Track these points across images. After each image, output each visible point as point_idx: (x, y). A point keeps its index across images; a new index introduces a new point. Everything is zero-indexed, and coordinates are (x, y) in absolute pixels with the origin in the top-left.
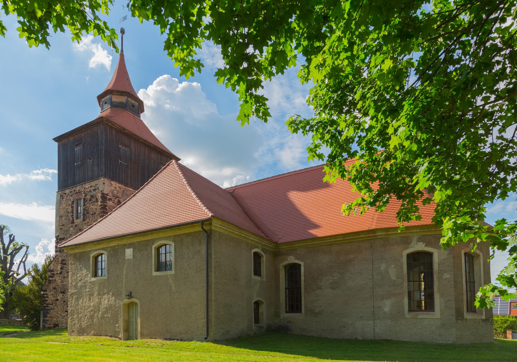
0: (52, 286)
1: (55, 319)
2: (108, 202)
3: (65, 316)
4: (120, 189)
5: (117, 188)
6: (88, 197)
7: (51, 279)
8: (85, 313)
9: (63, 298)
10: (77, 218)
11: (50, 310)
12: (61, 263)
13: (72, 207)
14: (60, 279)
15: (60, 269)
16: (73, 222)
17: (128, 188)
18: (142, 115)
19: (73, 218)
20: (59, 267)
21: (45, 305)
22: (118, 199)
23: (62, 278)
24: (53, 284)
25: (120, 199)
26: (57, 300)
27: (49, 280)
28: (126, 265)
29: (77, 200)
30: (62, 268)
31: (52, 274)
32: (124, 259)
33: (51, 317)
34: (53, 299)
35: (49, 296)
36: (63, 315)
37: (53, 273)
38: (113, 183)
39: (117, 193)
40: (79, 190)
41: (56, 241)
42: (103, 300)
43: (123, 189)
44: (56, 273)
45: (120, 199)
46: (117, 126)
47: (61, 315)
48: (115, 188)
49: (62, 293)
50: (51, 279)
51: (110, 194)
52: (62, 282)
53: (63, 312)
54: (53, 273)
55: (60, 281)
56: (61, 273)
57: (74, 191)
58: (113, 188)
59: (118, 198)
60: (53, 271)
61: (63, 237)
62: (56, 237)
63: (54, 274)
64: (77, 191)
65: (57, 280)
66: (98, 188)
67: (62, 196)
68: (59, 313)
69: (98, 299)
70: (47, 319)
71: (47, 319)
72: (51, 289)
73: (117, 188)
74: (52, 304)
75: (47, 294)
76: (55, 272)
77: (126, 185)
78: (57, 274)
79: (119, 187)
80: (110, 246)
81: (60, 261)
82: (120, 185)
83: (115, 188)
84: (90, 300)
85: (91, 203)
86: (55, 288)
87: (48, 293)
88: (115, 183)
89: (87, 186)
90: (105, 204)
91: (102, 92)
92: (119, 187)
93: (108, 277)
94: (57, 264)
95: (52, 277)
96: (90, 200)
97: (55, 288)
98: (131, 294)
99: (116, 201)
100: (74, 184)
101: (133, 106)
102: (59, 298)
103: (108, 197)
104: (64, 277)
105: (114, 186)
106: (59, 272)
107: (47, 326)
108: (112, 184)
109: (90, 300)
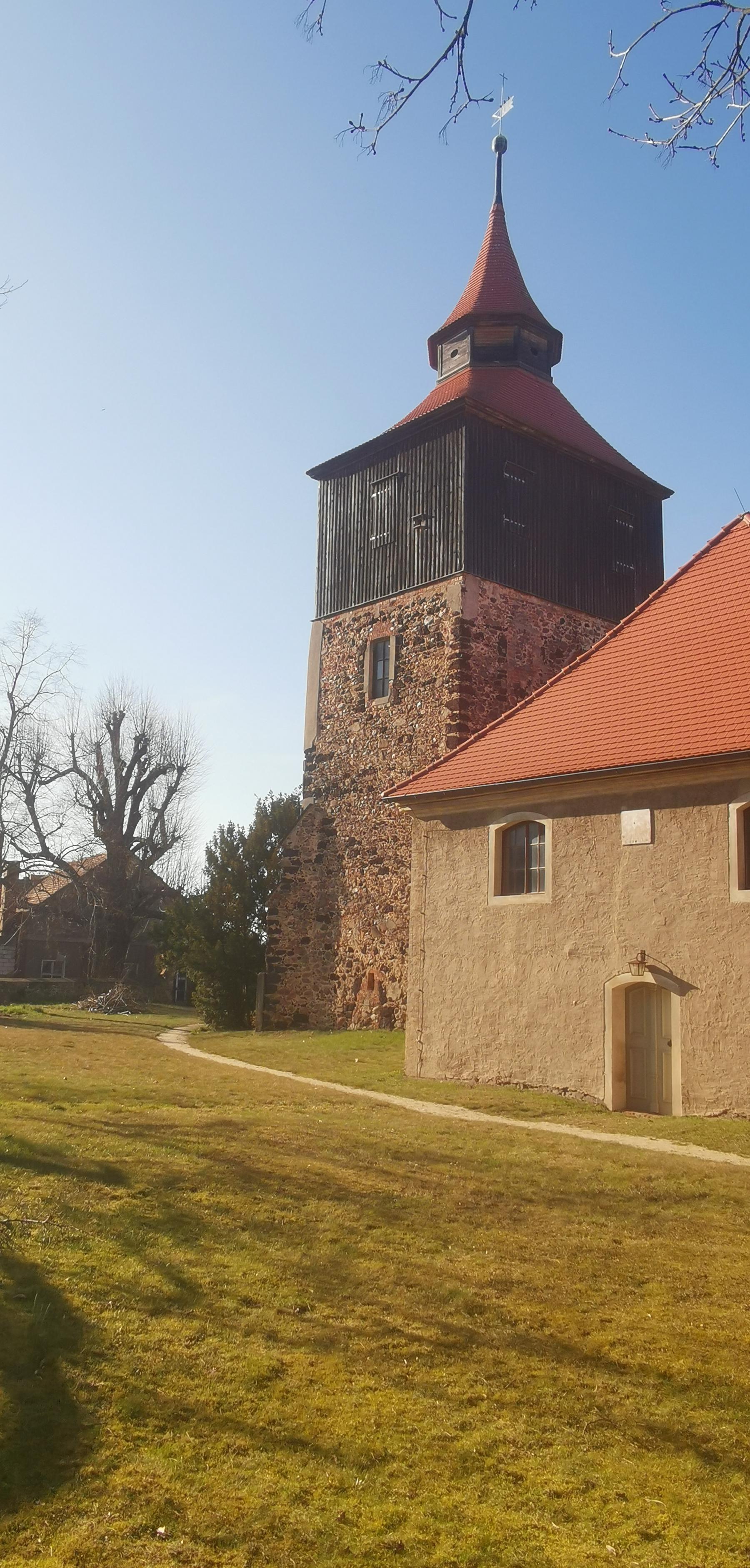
0: (293, 897)
1: (297, 998)
2: (473, 645)
3: (328, 992)
4: (506, 602)
5: (499, 601)
6: (413, 630)
7: (289, 876)
8: (468, 1008)
9: (323, 936)
10: (374, 695)
11: (284, 970)
12: (322, 831)
13: (361, 664)
14: (316, 879)
15: (316, 849)
16: (361, 708)
17: (528, 598)
18: (556, 371)
19: (362, 695)
20: (315, 841)
21: (271, 955)
22: (499, 632)
23: (322, 873)
24: (295, 892)
25: (506, 633)
26: (306, 940)
27: (284, 880)
28: (625, 862)
29: (375, 643)
30: (322, 845)
31: (293, 862)
32: (616, 843)
33: (287, 992)
34: (294, 936)
35: (283, 928)
36: (322, 987)
37: (295, 858)
38: (487, 585)
39: (499, 617)
40: (382, 613)
41: (306, 761)
42: (535, 971)
43: (513, 602)
44: (306, 858)
45: (506, 633)
46: (502, 417)
47: (316, 988)
48: (493, 600)
49: (320, 919)
50: (289, 876)
51: (480, 621)
52: (323, 885)
53: (325, 978)
54: (295, 858)
55: (315, 883)
56: (319, 859)
57: (368, 615)
58: (487, 602)
59: (500, 629)
60: (296, 853)
61: (327, 752)
62: (306, 752)
63: (298, 862)
64: (377, 615)
65: (307, 879)
66: (444, 605)
67: (329, 631)
68: (312, 980)
69: (517, 964)
70: (277, 996)
71: (277, 996)
72: (291, 906)
73: (499, 601)
74: (291, 954)
75: (277, 923)
76: (303, 857)
77: (521, 588)
78: (306, 862)
79: (503, 596)
80: (560, 798)
81: (317, 822)
82: (506, 591)
83: (493, 600)
84: (485, 966)
85: (424, 649)
86: (300, 905)
87: (279, 919)
88: (492, 585)
89: (409, 599)
90: (465, 651)
91: (436, 331)
92: (503, 596)
93: (554, 898)
94: (308, 832)
95: (293, 871)
96: (419, 641)
97: (300, 905)
98: (643, 958)
99: (495, 639)
100: (367, 594)
101: (535, 351)
102: (310, 934)
103: (474, 629)
104: (330, 872)
105: (491, 596)
106: (314, 856)
107: (274, 1019)
108: (484, 591)
109: (485, 966)
